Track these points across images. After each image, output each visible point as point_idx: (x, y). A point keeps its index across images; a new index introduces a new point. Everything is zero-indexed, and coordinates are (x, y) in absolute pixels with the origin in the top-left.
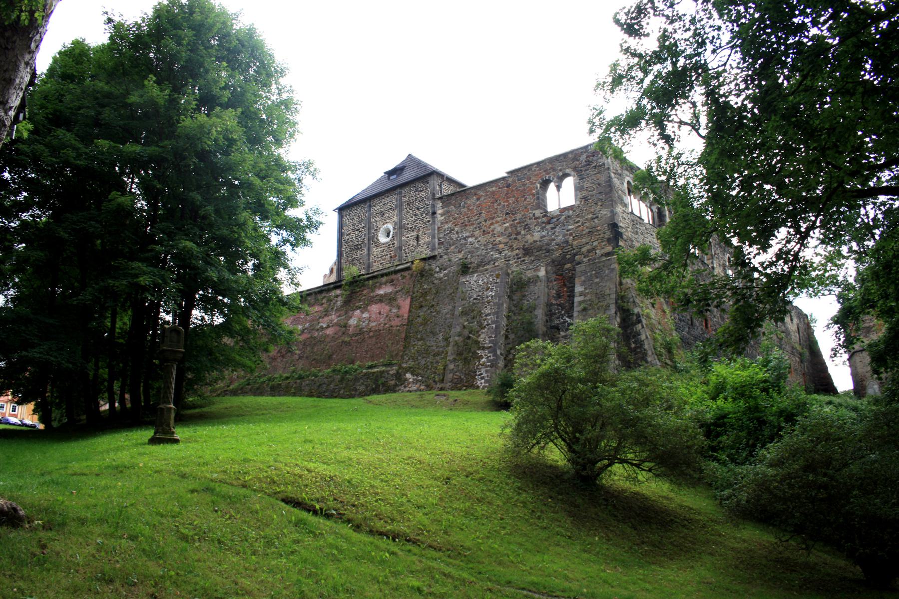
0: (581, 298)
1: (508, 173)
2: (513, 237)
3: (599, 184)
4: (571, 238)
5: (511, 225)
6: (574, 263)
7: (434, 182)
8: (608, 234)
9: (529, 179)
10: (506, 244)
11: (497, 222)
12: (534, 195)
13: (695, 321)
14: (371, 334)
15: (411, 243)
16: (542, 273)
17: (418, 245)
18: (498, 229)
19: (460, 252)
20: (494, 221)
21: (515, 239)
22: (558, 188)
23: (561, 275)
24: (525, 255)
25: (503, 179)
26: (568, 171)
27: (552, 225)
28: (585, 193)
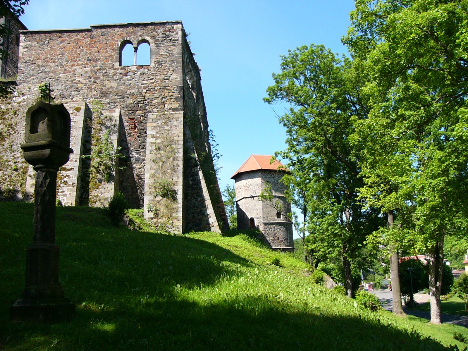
2: (93, 80)
10: (85, 84)
11: (78, 65)
13: (226, 296)
18: (79, 70)
20: (75, 63)
24: (102, 97)
26: (148, 38)
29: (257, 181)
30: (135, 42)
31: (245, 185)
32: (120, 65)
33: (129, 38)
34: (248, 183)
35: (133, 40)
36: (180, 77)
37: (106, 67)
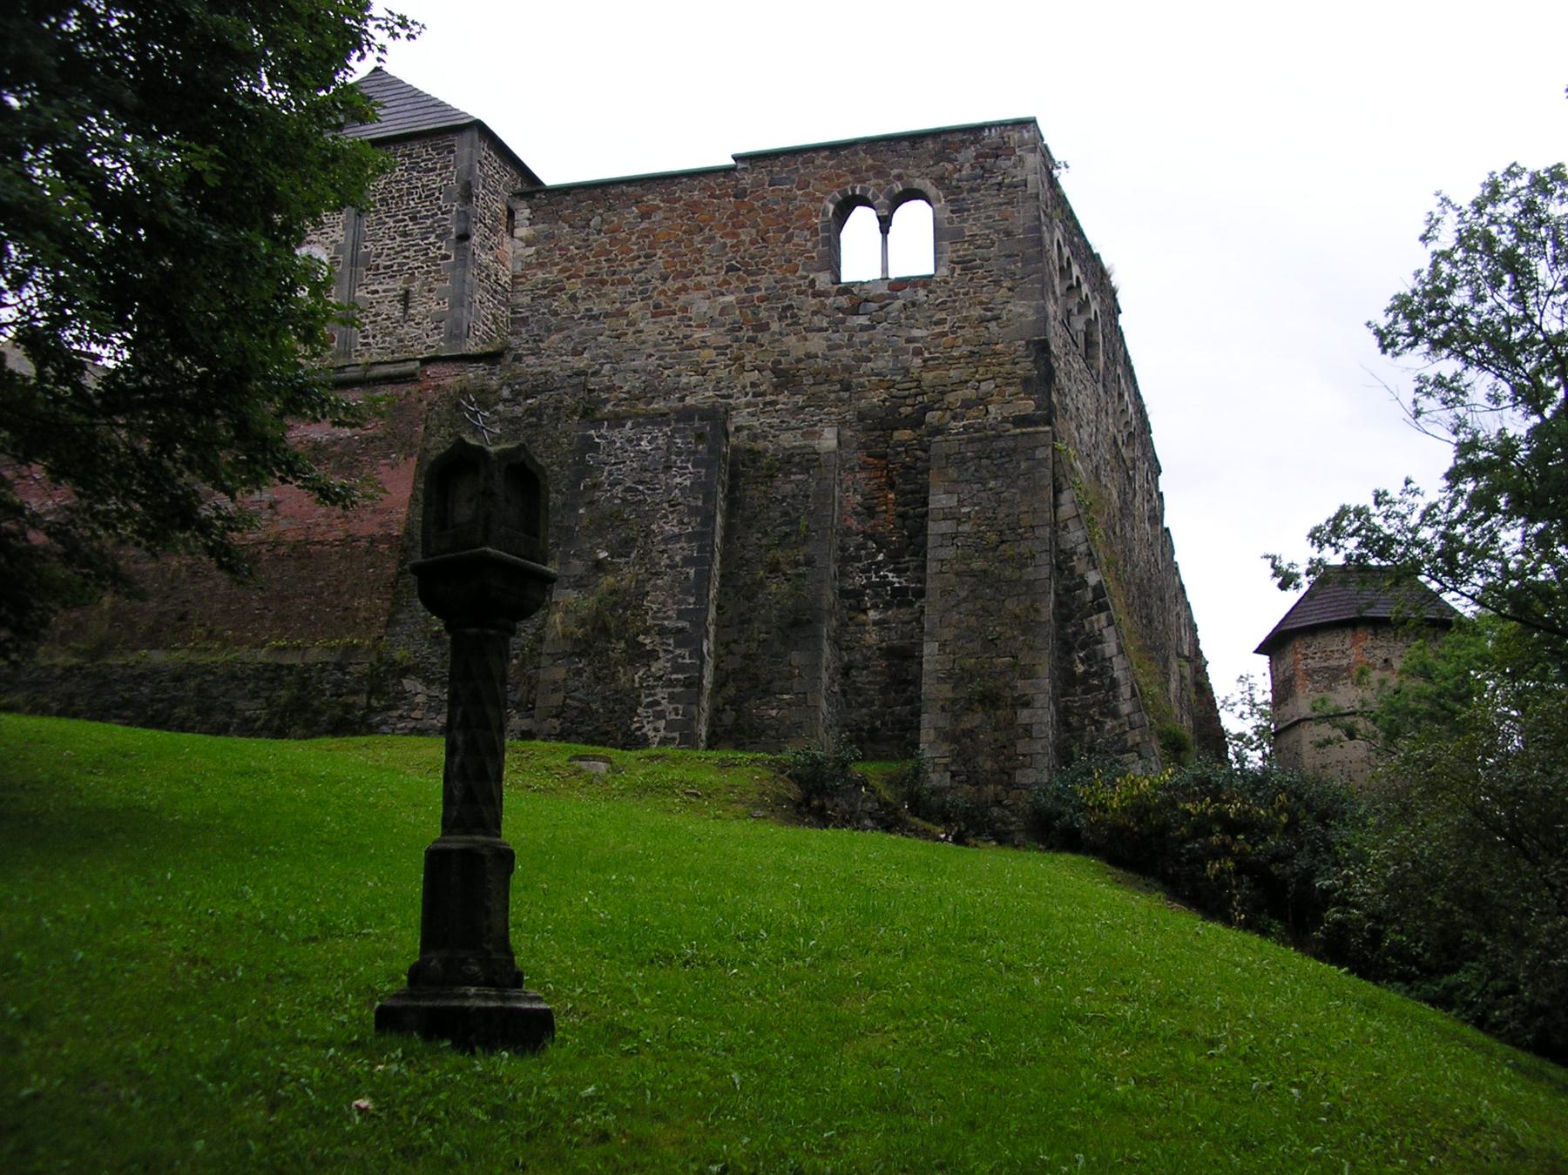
0: (946, 527)
1: (736, 158)
3: (1008, 234)
4: (918, 361)
5: (741, 302)
6: (923, 430)
7: (464, 147)
8: (1025, 367)
9: (803, 185)
10: (721, 350)
12: (815, 232)
14: (282, 550)
15: (385, 308)
16: (828, 440)
17: (407, 317)
18: (701, 306)
19: (576, 353)
20: (688, 282)
21: (751, 340)
22: (885, 224)
23: (884, 456)
24: (778, 388)
25: (726, 171)
26: (918, 183)
27: (863, 320)
28: (964, 250)
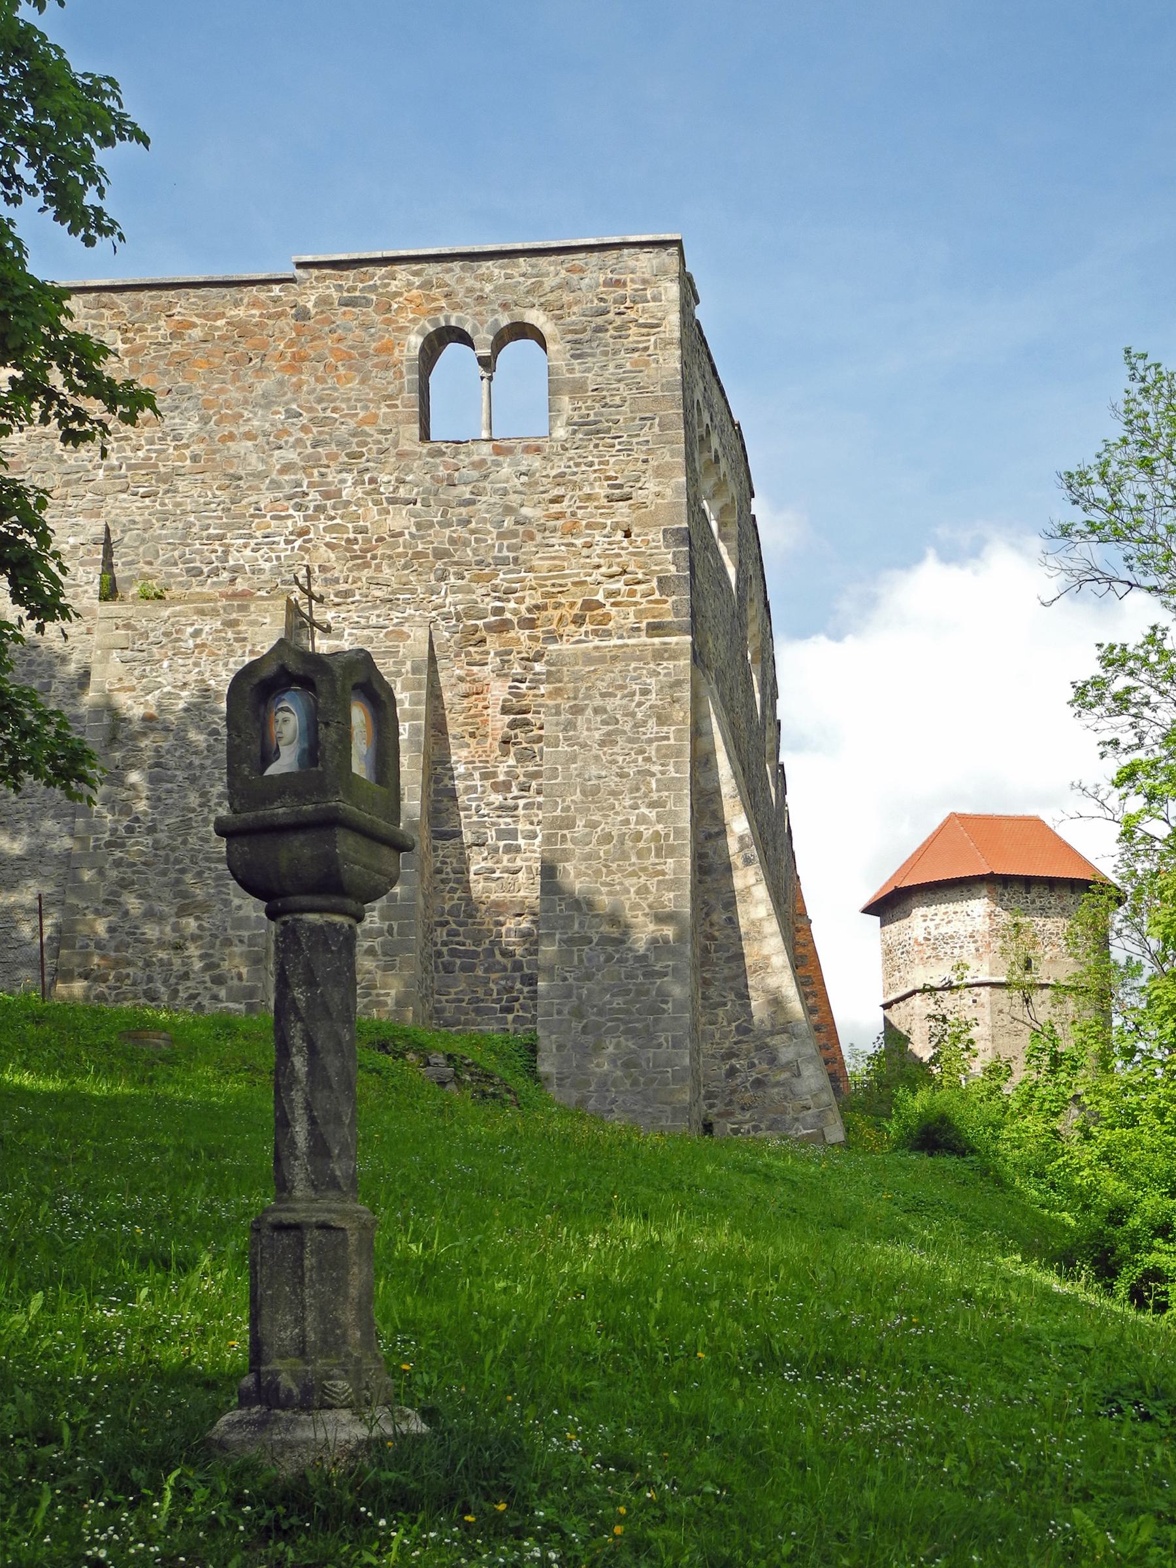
26: (536, 317)
29: (977, 911)
30: (484, 338)
31: (921, 940)
32: (425, 436)
33: (459, 319)
34: (934, 932)
35: (475, 328)
36: (676, 490)
37: (365, 444)
